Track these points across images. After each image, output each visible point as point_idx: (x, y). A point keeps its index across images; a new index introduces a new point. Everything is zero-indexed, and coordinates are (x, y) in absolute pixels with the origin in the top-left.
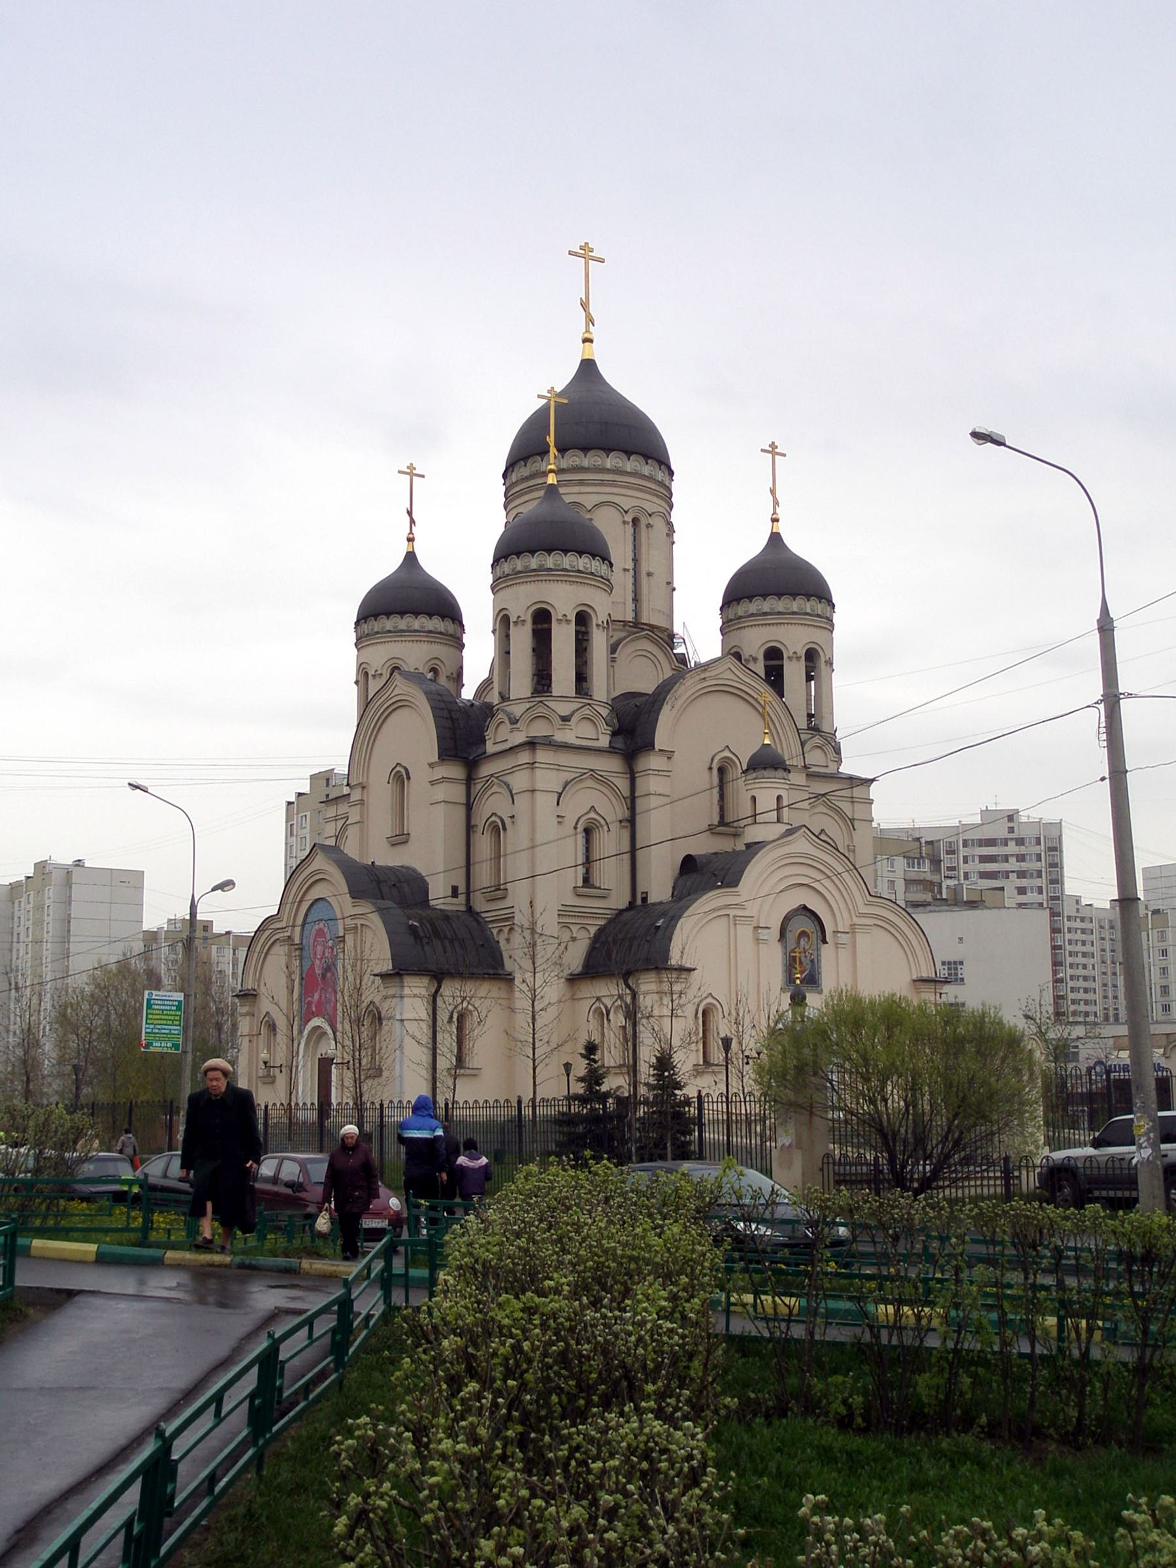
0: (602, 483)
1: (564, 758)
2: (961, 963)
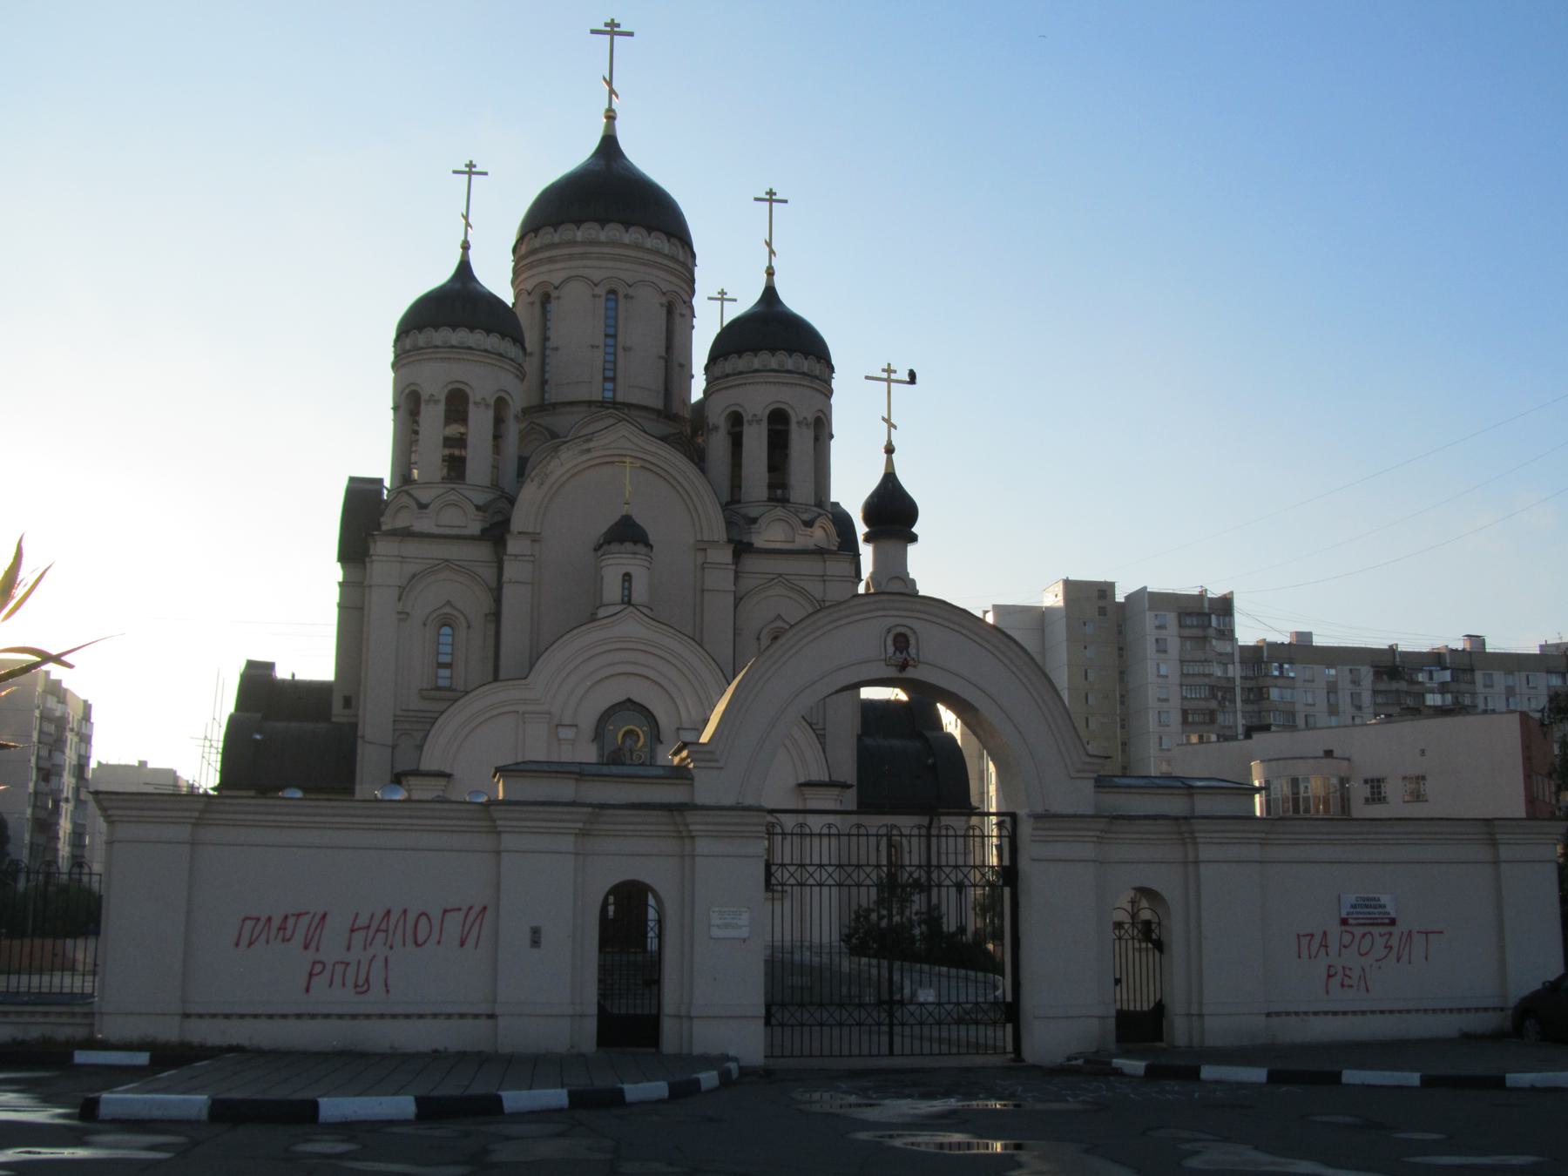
0: (571, 257)
1: (411, 548)
2: (1424, 778)
